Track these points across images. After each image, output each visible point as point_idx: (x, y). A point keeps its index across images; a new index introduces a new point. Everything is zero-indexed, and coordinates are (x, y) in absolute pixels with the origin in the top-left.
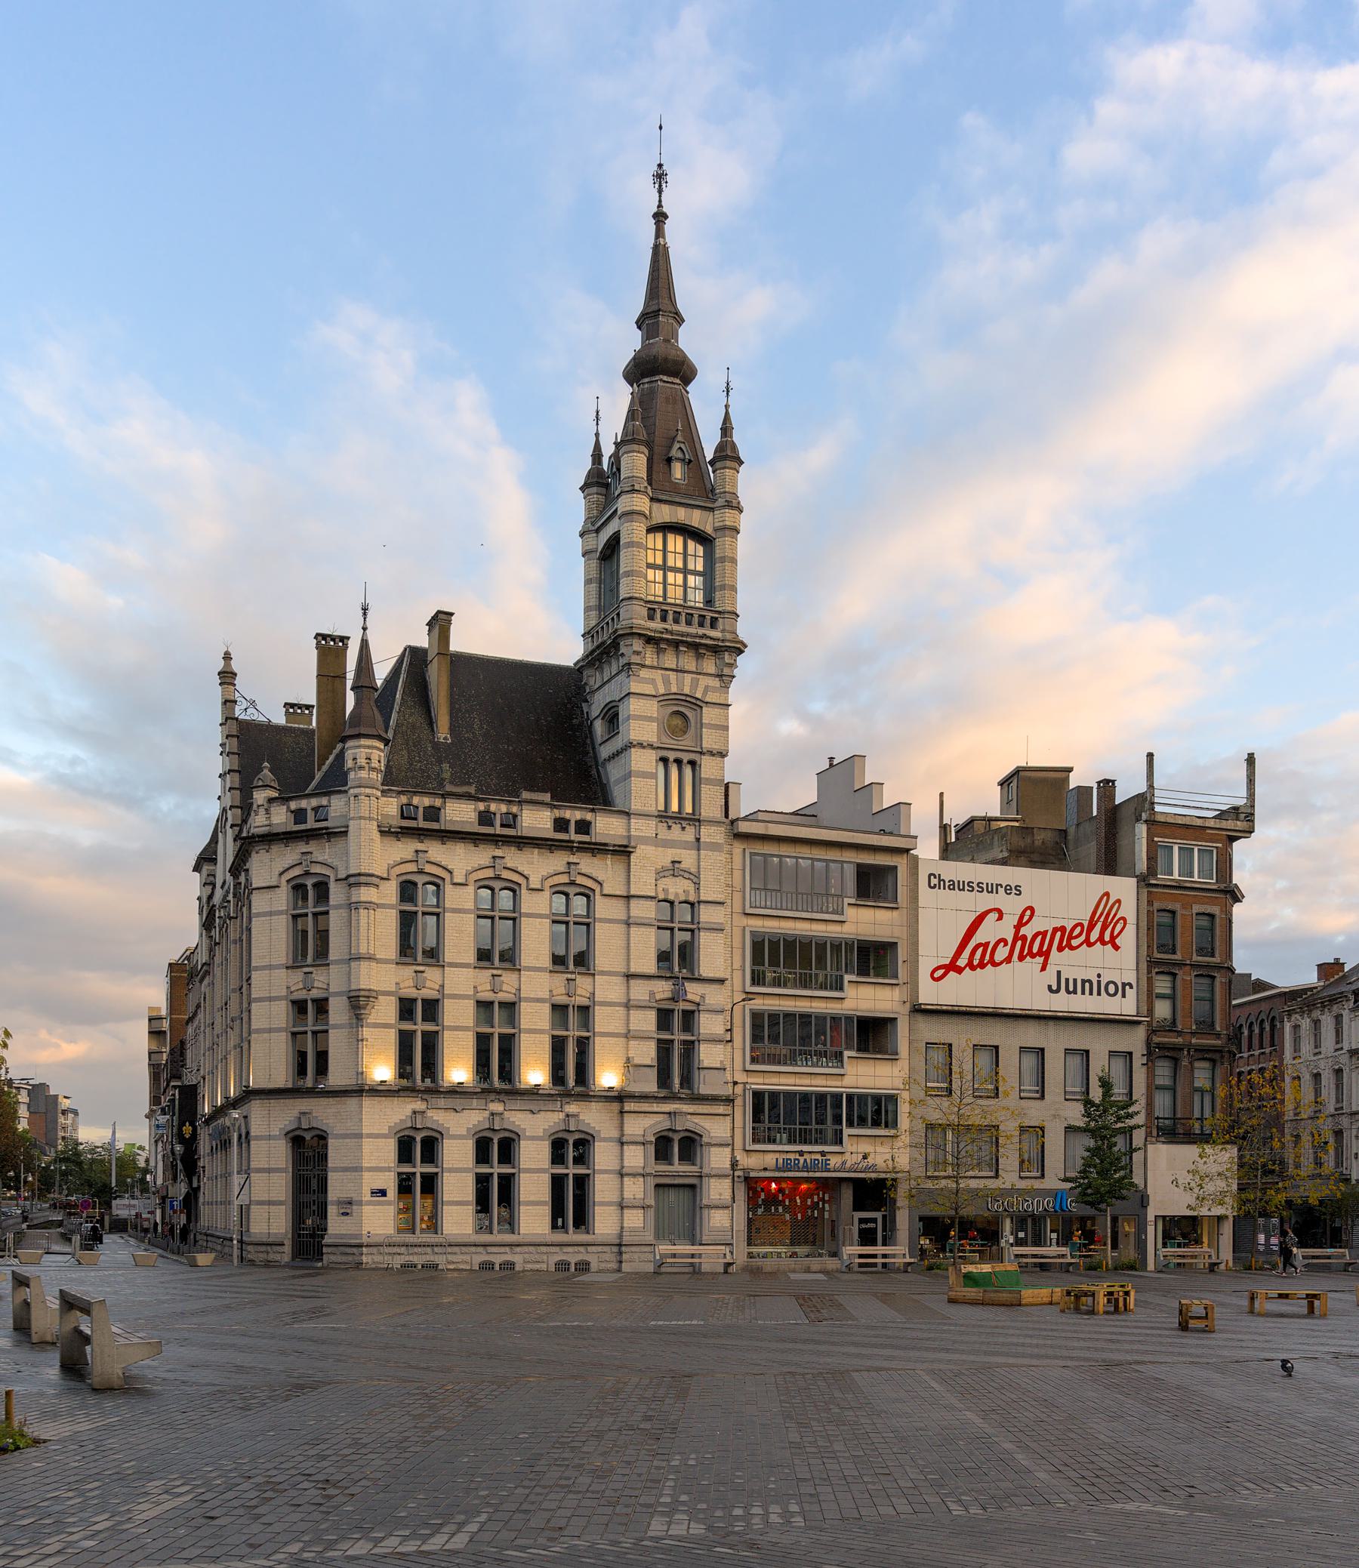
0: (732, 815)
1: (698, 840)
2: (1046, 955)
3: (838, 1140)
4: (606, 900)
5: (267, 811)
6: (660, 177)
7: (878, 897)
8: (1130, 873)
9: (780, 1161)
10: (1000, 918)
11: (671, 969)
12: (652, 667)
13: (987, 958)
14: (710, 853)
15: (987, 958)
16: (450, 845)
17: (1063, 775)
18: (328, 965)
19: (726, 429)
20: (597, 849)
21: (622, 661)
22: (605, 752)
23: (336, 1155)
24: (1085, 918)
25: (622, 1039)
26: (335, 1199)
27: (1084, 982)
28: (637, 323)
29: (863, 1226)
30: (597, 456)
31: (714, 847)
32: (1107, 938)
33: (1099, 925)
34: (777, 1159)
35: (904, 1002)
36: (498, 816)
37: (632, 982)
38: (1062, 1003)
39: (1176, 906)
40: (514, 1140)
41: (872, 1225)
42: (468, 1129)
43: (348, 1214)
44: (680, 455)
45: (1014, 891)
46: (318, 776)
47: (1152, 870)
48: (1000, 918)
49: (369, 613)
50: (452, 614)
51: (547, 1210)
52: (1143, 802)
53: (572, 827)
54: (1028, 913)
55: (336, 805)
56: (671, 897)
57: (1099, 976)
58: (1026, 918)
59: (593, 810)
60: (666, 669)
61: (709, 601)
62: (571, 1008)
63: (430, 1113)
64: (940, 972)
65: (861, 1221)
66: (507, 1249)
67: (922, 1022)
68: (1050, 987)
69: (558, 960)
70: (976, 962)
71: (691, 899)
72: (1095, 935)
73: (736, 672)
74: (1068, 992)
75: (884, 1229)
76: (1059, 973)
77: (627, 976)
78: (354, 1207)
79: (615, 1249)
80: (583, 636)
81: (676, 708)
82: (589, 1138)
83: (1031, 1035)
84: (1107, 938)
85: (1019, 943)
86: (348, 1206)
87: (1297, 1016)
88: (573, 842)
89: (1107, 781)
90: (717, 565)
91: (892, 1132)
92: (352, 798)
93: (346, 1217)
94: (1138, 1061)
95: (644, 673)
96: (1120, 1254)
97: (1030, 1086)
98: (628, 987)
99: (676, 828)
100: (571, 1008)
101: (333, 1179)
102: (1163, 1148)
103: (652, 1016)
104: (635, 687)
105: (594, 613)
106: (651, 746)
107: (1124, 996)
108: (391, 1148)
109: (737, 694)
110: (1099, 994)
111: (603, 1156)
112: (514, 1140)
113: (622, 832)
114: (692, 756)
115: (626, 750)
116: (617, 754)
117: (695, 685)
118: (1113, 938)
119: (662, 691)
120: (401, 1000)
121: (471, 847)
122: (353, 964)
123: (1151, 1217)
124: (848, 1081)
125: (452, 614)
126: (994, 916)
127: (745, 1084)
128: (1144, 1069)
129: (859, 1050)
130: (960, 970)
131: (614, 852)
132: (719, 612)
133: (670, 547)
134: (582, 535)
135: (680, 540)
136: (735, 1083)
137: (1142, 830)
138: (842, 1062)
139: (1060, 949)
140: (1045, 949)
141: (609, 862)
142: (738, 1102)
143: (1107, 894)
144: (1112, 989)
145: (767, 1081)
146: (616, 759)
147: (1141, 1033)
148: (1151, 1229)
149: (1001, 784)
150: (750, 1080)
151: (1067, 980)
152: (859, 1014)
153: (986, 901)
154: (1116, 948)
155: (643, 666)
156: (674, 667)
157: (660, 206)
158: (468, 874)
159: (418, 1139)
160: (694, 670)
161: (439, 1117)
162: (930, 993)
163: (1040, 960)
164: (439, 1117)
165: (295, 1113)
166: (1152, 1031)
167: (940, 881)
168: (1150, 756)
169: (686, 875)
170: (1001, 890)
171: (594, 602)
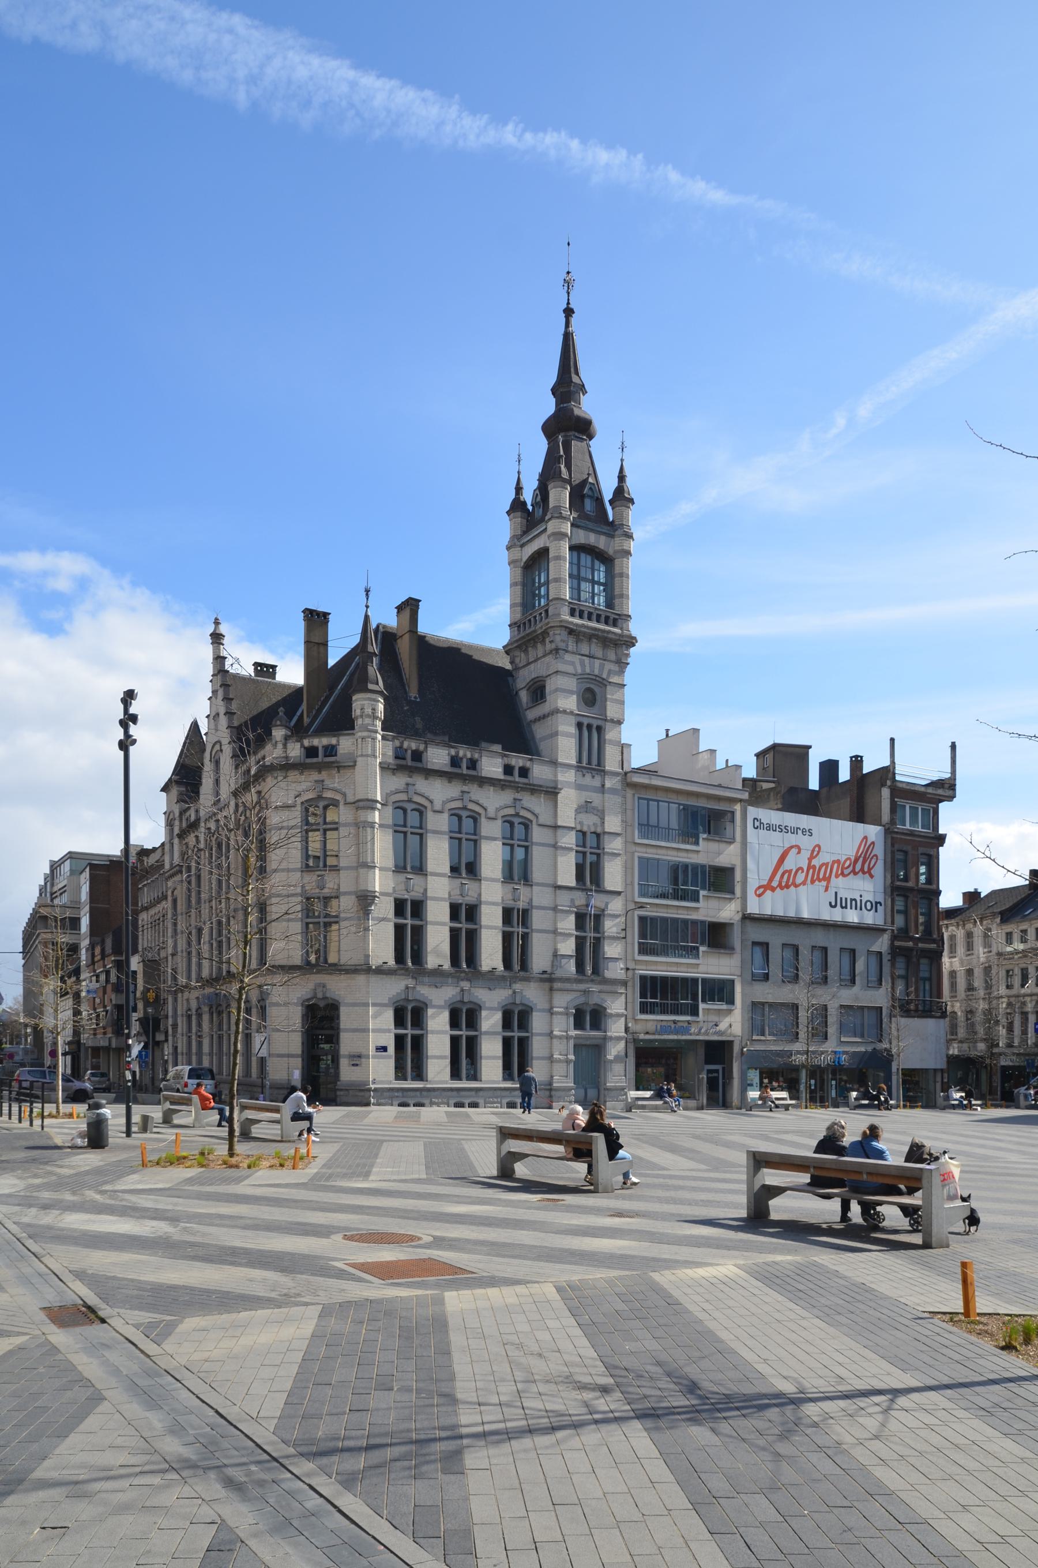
0: (626, 768)
1: (603, 786)
2: (828, 880)
3: (695, 1012)
4: (541, 829)
5: (285, 746)
6: (568, 284)
7: (717, 833)
8: (877, 822)
9: (659, 1027)
10: (799, 852)
11: (584, 884)
12: (573, 653)
13: (791, 880)
14: (612, 796)
15: (791, 880)
16: (431, 780)
17: (802, 751)
18: (339, 870)
19: (622, 478)
20: (534, 790)
21: (549, 646)
22: (531, 715)
23: (346, 1018)
24: (852, 853)
25: (551, 935)
26: (347, 1053)
27: (852, 900)
28: (552, 390)
29: (710, 1075)
30: (519, 489)
31: (613, 791)
32: (866, 869)
33: (861, 859)
36: (465, 760)
37: (558, 892)
38: (836, 915)
39: (908, 848)
40: (476, 1010)
41: (715, 1075)
42: (445, 1001)
43: (357, 1065)
44: (590, 493)
45: (808, 833)
47: (893, 822)
48: (799, 852)
49: (371, 594)
50: (420, 601)
51: (500, 1063)
52: (886, 774)
53: (516, 772)
54: (817, 849)
55: (345, 744)
56: (585, 829)
57: (861, 896)
58: (815, 853)
59: (531, 760)
60: (583, 655)
61: (610, 604)
62: (588, 916)
63: (418, 988)
64: (761, 890)
65: (709, 1071)
66: (473, 1093)
67: (751, 928)
68: (830, 903)
69: (455, 870)
70: (783, 884)
71: (599, 830)
72: (858, 867)
73: (629, 660)
74: (842, 907)
75: (724, 1078)
76: (836, 893)
77: (555, 887)
78: (363, 1060)
79: (547, 1093)
80: (510, 626)
81: (588, 686)
82: (477, 1008)
83: (819, 938)
84: (866, 869)
85: (811, 871)
86: (358, 1059)
87: (954, 928)
88: (517, 783)
89: (856, 757)
90: (616, 579)
92: (360, 740)
93: (355, 1068)
94: (886, 958)
95: (568, 657)
97: (874, 978)
98: (555, 895)
99: (588, 776)
100: (588, 916)
101: (344, 1037)
102: (903, 1021)
103: (572, 918)
104: (562, 667)
105: (519, 609)
106: (572, 713)
107: (876, 911)
108: (389, 1015)
109: (630, 676)
110: (861, 909)
111: (538, 1022)
112: (422, 1009)
113: (551, 777)
114: (600, 723)
115: (552, 715)
116: (544, 717)
117: (602, 667)
118: (870, 869)
119: (579, 671)
120: (396, 900)
121: (446, 782)
122: (362, 871)
123: (894, 1069)
124: (701, 968)
125: (420, 601)
126: (794, 851)
127: (634, 970)
128: (889, 964)
130: (773, 889)
131: (547, 792)
132: (619, 615)
133: (582, 563)
134: (508, 548)
135: (589, 558)
136: (628, 969)
137: (886, 792)
138: (698, 955)
139: (837, 876)
140: (827, 875)
141: (542, 800)
142: (629, 984)
143: (866, 838)
144: (869, 906)
145: (679, 970)
146: (542, 721)
147: (886, 939)
148: (894, 1078)
149: (758, 755)
150: (637, 967)
151: (841, 899)
152: (710, 919)
153: (791, 839)
154: (872, 876)
155: (567, 651)
156: (587, 653)
157: (568, 303)
158: (444, 803)
159: (410, 1008)
160: (601, 656)
161: (426, 992)
162: (754, 907)
163: (824, 883)
164: (426, 992)
165: (311, 986)
166: (894, 938)
167: (761, 823)
168: (892, 740)
169: (595, 812)
170: (800, 832)
171: (519, 600)
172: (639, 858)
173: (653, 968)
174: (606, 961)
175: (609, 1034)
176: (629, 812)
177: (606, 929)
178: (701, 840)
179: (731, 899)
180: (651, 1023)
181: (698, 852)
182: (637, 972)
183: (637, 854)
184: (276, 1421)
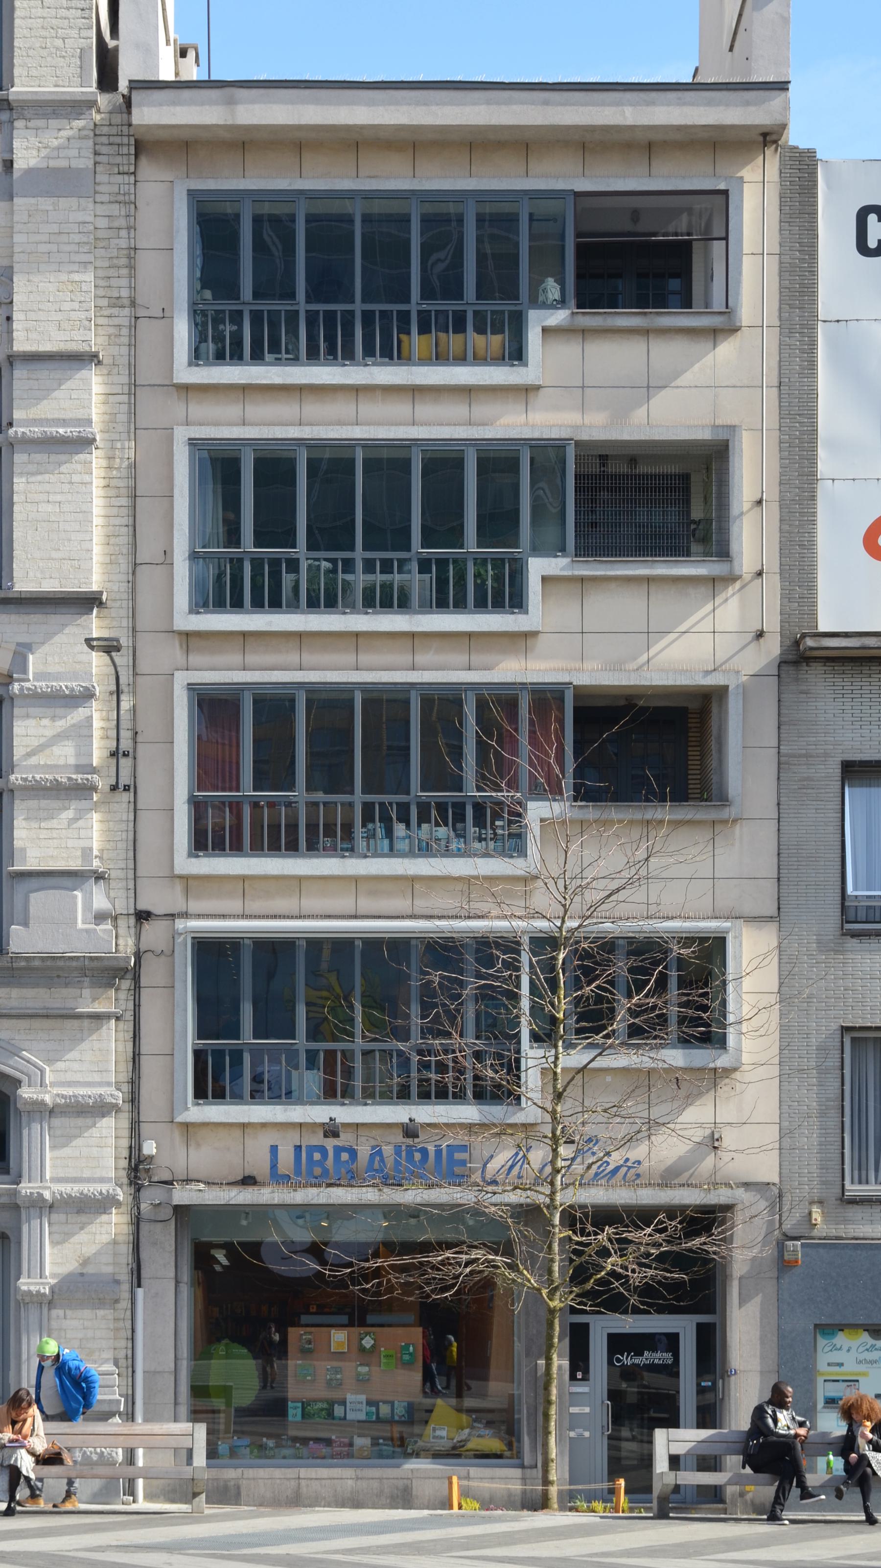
14: (45, 203)
34: (274, 1149)
35: (760, 635)
41: (661, 1357)
46: (483, 982)
91: (701, 1056)
96: (140, 1424)
129: (583, 794)
136: (142, 916)
142: (152, 973)
172: (193, 443)
173: (281, 904)
174: (21, 888)
175: (26, 1188)
176: (147, 263)
177: (18, 752)
178: (533, 337)
179: (715, 583)
180: (266, 1140)
181: (527, 391)
182: (180, 924)
183: (181, 434)
184: (777, 1006)
